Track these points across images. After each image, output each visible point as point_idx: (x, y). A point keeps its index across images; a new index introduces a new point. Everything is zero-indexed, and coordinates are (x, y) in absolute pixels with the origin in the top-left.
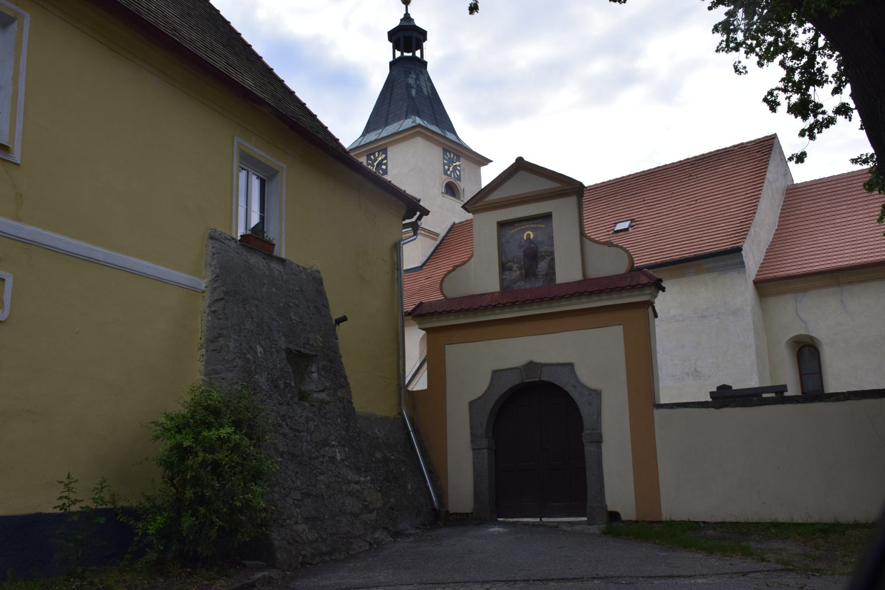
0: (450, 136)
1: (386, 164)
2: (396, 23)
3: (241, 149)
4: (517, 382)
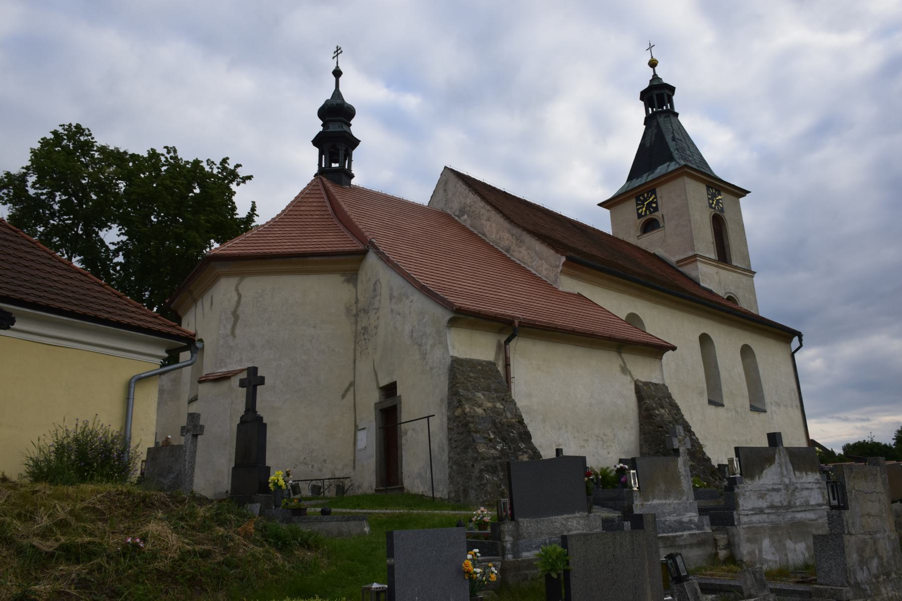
1: (656, 203)
2: (646, 85)
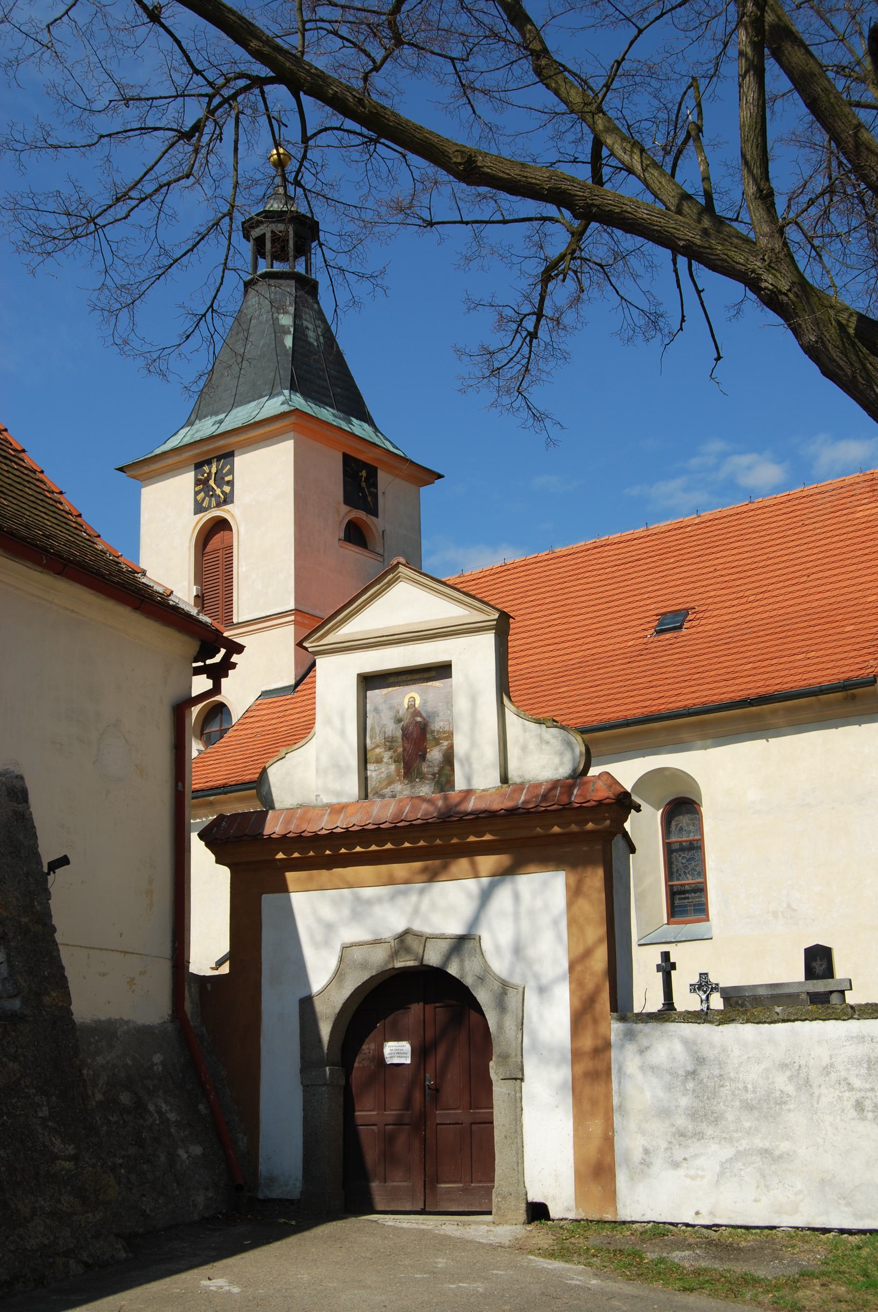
0: (359, 428)
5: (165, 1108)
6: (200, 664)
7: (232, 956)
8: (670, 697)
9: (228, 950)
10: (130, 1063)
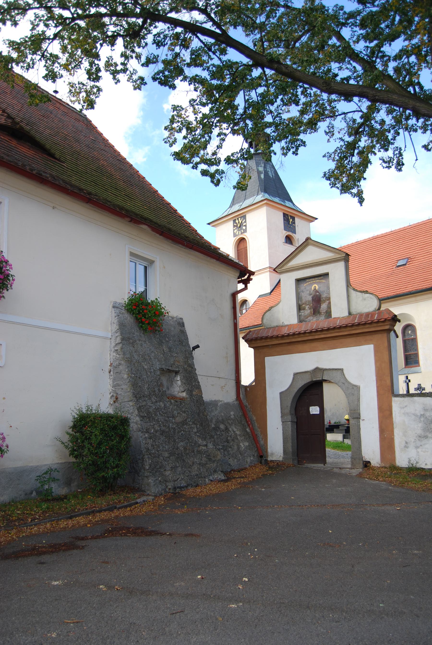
0: (288, 204)
1: (246, 226)
3: (130, 252)
4: (309, 380)
5: (236, 430)
6: (240, 279)
7: (255, 380)
8: (403, 288)
9: (254, 378)
10: (223, 415)
